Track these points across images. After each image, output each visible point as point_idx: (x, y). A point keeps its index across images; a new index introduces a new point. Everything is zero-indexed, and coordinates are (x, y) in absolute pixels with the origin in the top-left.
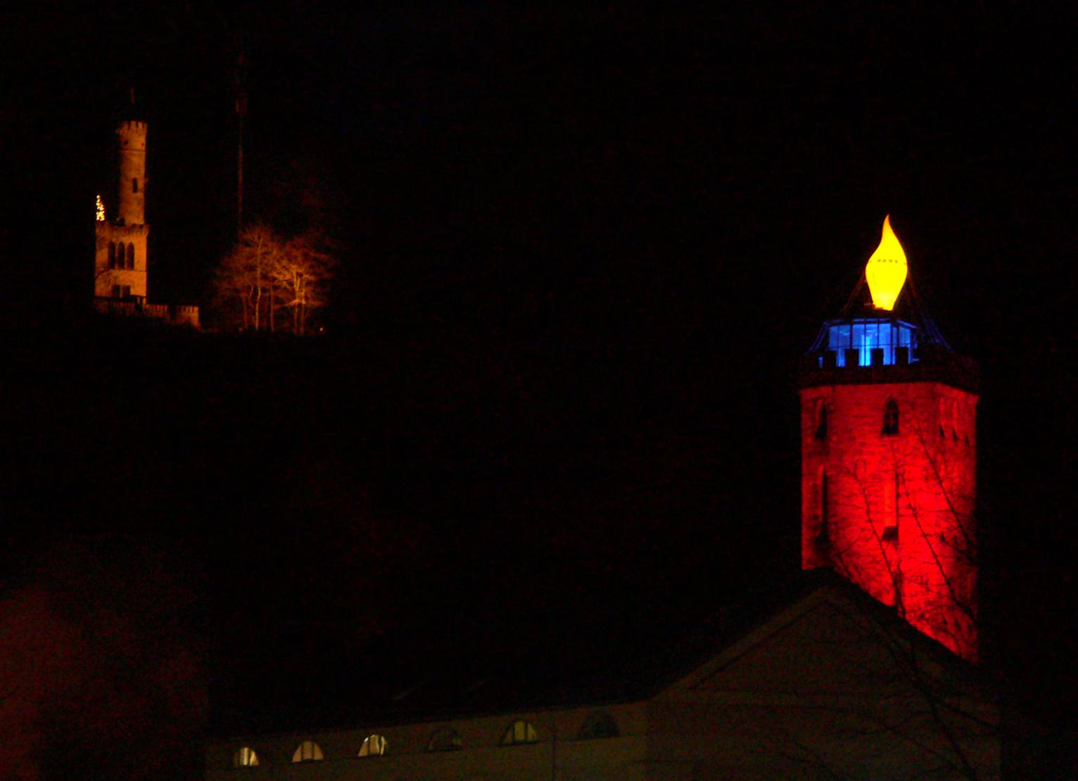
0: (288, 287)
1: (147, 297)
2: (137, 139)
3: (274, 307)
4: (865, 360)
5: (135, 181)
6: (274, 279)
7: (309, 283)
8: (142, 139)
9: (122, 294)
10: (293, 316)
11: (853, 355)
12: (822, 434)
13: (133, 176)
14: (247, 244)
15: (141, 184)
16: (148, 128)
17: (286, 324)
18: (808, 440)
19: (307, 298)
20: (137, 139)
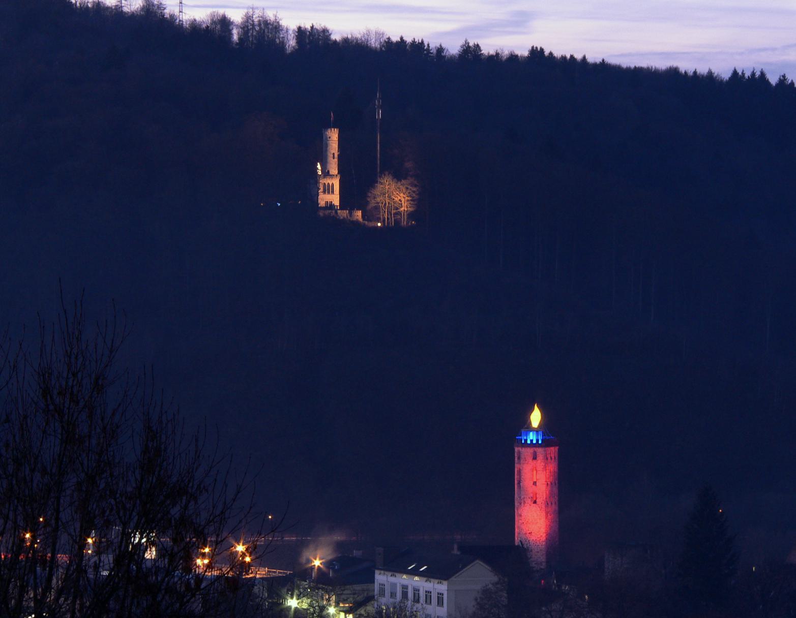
0: (400, 202)
1: (340, 206)
2: (333, 135)
3: (393, 212)
4: (529, 442)
5: (334, 154)
6: (393, 199)
7: (408, 200)
8: (337, 136)
9: (330, 206)
10: (401, 214)
11: (526, 440)
12: (519, 458)
13: (333, 152)
14: (382, 184)
15: (336, 156)
16: (339, 131)
17: (399, 217)
18: (516, 459)
19: (407, 207)
20: (333, 135)
